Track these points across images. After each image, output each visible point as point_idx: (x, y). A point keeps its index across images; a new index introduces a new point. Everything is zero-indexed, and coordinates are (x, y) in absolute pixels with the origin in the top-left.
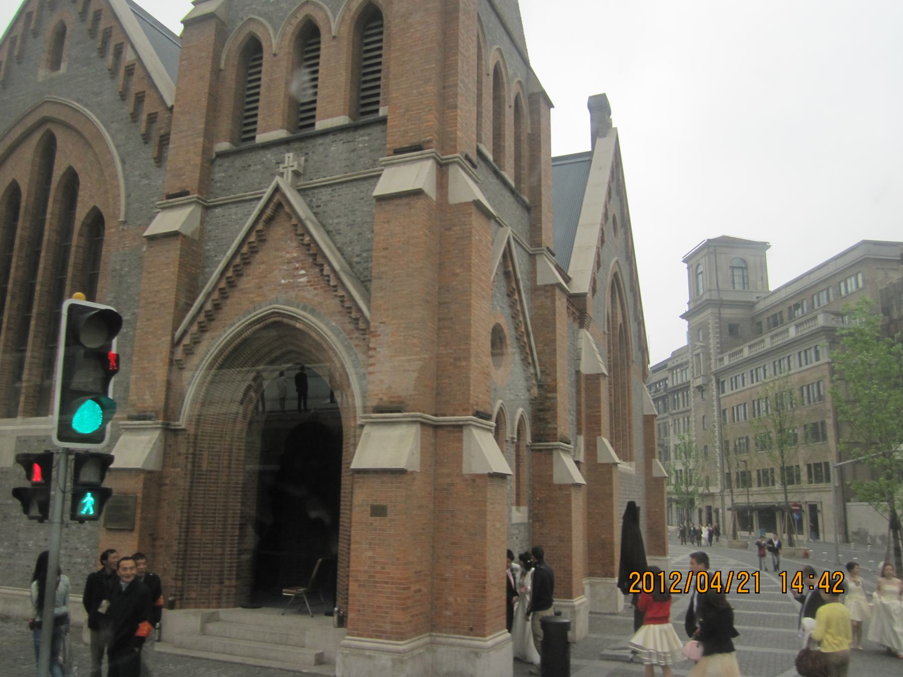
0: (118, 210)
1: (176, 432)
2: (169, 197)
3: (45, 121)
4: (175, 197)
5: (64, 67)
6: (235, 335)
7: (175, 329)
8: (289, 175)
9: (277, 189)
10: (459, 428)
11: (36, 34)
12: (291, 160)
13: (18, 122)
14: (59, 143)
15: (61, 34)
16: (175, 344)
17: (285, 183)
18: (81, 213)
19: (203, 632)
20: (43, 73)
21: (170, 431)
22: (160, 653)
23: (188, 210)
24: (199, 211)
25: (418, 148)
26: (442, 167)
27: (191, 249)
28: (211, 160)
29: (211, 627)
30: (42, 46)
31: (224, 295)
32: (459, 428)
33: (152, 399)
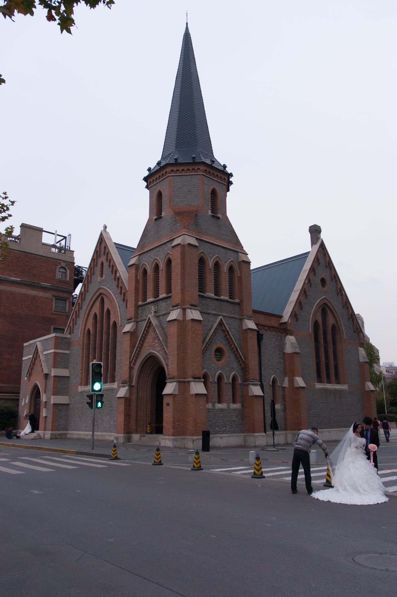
0: (119, 324)
1: (133, 386)
2: (128, 320)
3: (101, 294)
4: (129, 320)
5: (104, 276)
6: (82, 331)
7: (130, 358)
8: (153, 314)
9: (149, 318)
10: (189, 382)
11: (97, 266)
12: (153, 308)
13: (95, 294)
14: (105, 301)
15: (102, 263)
16: (130, 363)
17: (151, 316)
18: (111, 323)
19: (140, 439)
20: (99, 278)
21: (131, 386)
22: (70, 278)
23: (132, 324)
24: (182, 310)
25: (177, 306)
26: (184, 310)
27: (133, 334)
28: (137, 307)
29: (142, 438)
30: (98, 269)
31: (141, 348)
32: (189, 382)
33: (126, 376)
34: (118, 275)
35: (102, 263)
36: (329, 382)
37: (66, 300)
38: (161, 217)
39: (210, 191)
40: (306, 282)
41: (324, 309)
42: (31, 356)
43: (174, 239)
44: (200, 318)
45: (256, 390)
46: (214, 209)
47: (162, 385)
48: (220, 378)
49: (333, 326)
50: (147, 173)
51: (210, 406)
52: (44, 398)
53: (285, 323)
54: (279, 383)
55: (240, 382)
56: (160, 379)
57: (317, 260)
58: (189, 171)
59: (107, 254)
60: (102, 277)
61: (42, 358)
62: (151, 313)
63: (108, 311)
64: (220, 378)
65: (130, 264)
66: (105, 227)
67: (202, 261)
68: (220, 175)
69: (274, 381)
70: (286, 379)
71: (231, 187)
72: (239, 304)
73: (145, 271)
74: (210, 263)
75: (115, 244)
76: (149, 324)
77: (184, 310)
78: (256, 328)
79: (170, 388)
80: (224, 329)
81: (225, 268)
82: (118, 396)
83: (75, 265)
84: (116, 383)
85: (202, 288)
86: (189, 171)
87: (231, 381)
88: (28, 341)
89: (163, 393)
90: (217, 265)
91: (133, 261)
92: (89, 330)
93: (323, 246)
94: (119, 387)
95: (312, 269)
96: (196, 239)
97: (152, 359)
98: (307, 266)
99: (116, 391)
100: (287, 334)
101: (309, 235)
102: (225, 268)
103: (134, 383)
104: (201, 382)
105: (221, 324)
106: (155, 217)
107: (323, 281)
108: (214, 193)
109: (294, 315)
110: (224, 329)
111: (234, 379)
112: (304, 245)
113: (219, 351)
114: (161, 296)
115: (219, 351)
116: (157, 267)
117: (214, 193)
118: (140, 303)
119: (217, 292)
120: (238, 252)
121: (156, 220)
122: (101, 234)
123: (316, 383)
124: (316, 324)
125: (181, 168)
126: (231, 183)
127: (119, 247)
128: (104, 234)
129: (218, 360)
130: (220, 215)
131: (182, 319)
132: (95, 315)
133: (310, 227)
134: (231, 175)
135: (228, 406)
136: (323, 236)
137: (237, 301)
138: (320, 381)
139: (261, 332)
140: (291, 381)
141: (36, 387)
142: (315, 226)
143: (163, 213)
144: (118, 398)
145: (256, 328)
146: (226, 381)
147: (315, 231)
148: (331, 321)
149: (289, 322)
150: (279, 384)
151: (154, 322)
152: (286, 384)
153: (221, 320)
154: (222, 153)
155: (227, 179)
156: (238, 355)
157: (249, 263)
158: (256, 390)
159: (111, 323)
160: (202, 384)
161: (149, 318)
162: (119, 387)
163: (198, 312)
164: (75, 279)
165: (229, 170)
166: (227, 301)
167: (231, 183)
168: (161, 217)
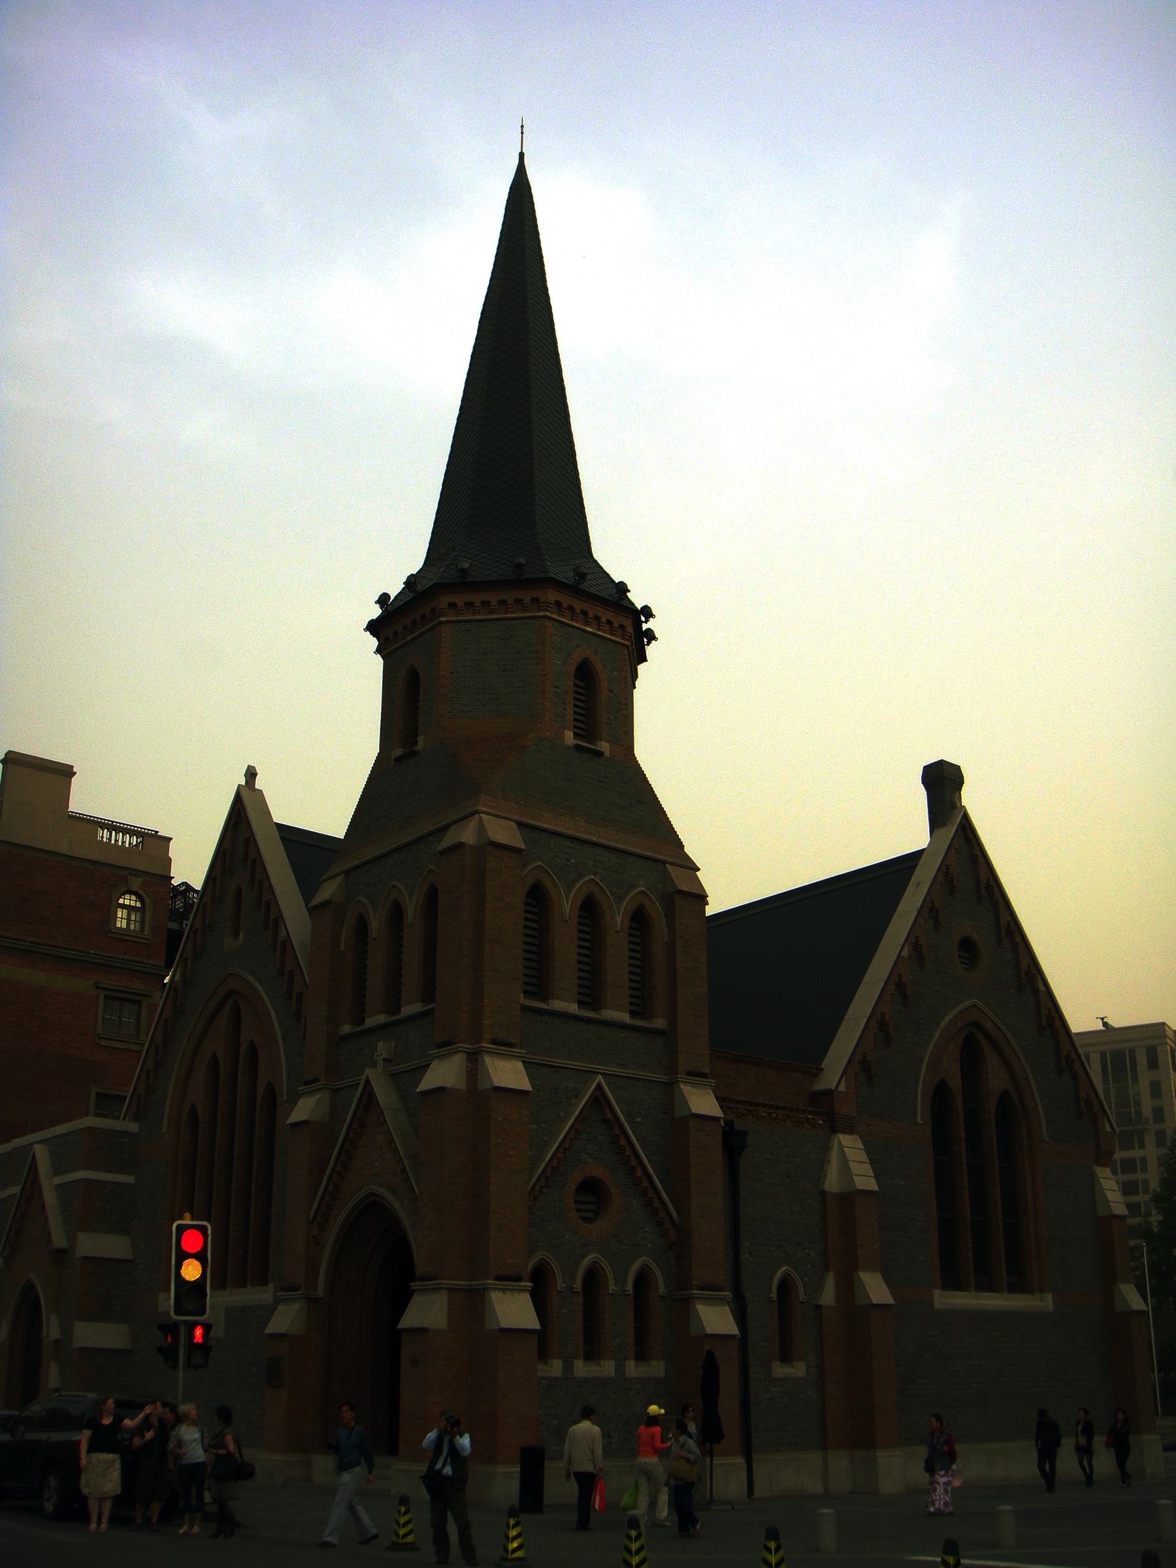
5: (241, 934)
12: (383, 1049)
15: (239, 893)
18: (261, 1088)
23: (316, 1097)
34: (283, 934)
35: (239, 893)
36: (986, 1285)
37: (139, 1003)
38: (413, 754)
39: (572, 669)
40: (905, 953)
41: (972, 1045)
42: (17, 1189)
43: (446, 828)
44: (525, 1084)
45: (716, 1319)
46: (588, 728)
47: (400, 1301)
48: (593, 1277)
49: (1004, 1097)
50: (376, 612)
51: (556, 1368)
52: (52, 1329)
53: (828, 1093)
54: (801, 1292)
55: (662, 1289)
56: (399, 1281)
57: (946, 878)
58: (511, 597)
59: (255, 863)
60: (237, 936)
61: (50, 1198)
62: (374, 1065)
63: (253, 1050)
64: (593, 1277)
65: (318, 899)
66: (251, 774)
67: (537, 896)
68: (606, 615)
69: (785, 1286)
70: (830, 1282)
71: (651, 650)
72: (662, 1033)
73: (362, 926)
74: (567, 905)
75: (281, 828)
76: (369, 1095)
77: (474, 1059)
78: (720, 1114)
79: (427, 1311)
80: (609, 1116)
81: (618, 919)
82: (271, 1329)
83: (175, 882)
84: (271, 1286)
85: (538, 983)
86: (511, 597)
87: (630, 1288)
88: (9, 1140)
89: (404, 1323)
90: (590, 908)
91: (327, 891)
92: (193, 1111)
93: (967, 835)
94: (277, 1301)
95: (930, 911)
96: (520, 824)
97: (373, 1208)
98: (912, 900)
99: (267, 1312)
100: (833, 1129)
101: (921, 794)
102: (618, 919)
103: (320, 1292)
104: (523, 1291)
105: (599, 1100)
106: (398, 752)
107: (968, 946)
108: (585, 673)
109: (862, 1066)
110: (609, 1116)
111: (643, 1279)
112: (907, 830)
113: (592, 1193)
114: (407, 1010)
115: (592, 1193)
116: (397, 912)
117: (585, 673)
118: (347, 1029)
119: (591, 995)
120: (664, 862)
121: (398, 760)
122: (238, 798)
123: (937, 1293)
124: (940, 1095)
125: (477, 599)
126: (651, 636)
127: (293, 838)
128: (245, 795)
129: (588, 1220)
130: (605, 747)
131: (462, 1086)
132: (214, 1060)
133: (927, 769)
134: (647, 612)
135: (620, 1368)
136: (971, 798)
137: (660, 1023)
138: (953, 1282)
139: (739, 1125)
140: (848, 1287)
141: (30, 1288)
142: (941, 764)
143: (421, 741)
144: (271, 1336)
145: (720, 1114)
146: (612, 1287)
147: (942, 781)
148: (996, 1080)
149: (842, 1088)
150: (802, 1296)
151: (385, 1094)
152: (828, 1296)
153: (599, 1086)
154: (620, 542)
155: (630, 629)
156: (657, 1204)
157: (701, 898)
158: (716, 1319)
159: (261, 1088)
160: (527, 1297)
161: (368, 1081)
162: (277, 1301)
163: (520, 1065)
164: (170, 931)
165: (638, 598)
166: (623, 1026)
167: (651, 636)
168: (413, 754)
